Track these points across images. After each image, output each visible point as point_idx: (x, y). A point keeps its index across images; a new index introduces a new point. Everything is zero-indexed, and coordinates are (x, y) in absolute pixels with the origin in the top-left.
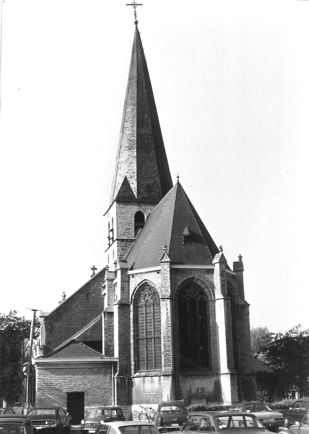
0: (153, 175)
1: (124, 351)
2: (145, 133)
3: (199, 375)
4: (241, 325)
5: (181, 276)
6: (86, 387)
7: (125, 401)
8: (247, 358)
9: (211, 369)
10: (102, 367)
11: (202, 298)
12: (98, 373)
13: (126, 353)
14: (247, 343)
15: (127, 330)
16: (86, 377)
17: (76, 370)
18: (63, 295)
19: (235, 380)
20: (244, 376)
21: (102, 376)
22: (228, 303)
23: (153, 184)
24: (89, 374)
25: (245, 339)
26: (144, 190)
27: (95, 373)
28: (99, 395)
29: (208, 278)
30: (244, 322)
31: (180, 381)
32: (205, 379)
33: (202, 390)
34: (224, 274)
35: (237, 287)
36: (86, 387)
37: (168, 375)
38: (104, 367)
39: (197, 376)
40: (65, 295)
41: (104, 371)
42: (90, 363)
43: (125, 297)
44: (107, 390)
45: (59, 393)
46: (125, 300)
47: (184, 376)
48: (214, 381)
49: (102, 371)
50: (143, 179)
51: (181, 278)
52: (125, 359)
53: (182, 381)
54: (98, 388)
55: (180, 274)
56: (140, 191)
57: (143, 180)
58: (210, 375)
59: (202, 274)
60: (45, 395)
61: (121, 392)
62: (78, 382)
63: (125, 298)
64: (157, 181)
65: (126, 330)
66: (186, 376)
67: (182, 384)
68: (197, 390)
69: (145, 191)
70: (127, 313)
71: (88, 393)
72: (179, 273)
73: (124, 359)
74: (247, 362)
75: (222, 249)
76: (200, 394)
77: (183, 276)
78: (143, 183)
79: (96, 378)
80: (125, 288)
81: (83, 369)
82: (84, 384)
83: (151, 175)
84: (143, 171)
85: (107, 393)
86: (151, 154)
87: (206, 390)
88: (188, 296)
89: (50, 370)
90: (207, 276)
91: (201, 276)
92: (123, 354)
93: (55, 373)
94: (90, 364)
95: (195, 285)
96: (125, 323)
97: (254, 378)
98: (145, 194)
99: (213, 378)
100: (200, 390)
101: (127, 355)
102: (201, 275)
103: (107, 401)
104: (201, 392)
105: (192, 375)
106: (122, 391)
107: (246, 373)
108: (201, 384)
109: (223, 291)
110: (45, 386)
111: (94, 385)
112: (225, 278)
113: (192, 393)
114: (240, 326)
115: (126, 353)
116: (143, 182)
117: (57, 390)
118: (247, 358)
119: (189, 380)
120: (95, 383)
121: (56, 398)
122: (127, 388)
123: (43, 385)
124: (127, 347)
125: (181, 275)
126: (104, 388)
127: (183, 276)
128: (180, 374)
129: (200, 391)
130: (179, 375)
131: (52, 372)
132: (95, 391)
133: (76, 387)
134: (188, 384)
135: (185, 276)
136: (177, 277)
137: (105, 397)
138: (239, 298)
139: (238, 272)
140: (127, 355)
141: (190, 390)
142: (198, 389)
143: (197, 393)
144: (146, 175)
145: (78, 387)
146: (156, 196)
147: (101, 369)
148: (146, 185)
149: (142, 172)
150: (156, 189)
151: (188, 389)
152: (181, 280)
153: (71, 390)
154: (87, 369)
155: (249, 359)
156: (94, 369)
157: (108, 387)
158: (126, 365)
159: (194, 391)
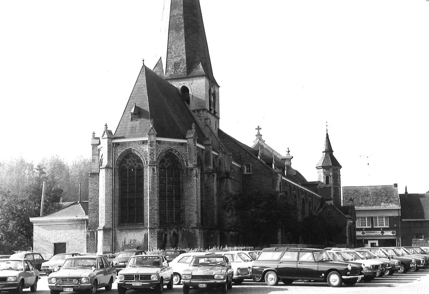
0: (181, 53)
1: (94, 210)
2: (177, 14)
3: (133, 229)
4: (190, 185)
5: (121, 149)
6: (67, 239)
7: (94, 249)
8: (193, 213)
9: (143, 225)
10: (79, 223)
11: (139, 166)
12: (76, 228)
13: (96, 212)
14: (193, 201)
15: (97, 193)
16: (67, 231)
17: (60, 226)
18: (287, 150)
19: (155, 233)
20: (190, 229)
21: (78, 231)
22: (153, 169)
23: (180, 61)
24: (70, 229)
25: (192, 197)
26: (172, 67)
27: (74, 228)
28: (77, 245)
29: (143, 149)
30: (192, 182)
31: (117, 234)
32: (137, 232)
33: (134, 241)
34: (153, 144)
35: (188, 152)
36: (67, 239)
37: (101, 230)
38: (80, 223)
39: (131, 230)
40: (289, 150)
41: (80, 226)
42: (69, 221)
43: (96, 167)
44: (82, 241)
45: (48, 244)
46: (96, 169)
47: (120, 230)
48: (144, 234)
49: (79, 227)
50: (172, 58)
51: (121, 150)
52: (94, 216)
53: (119, 234)
54: (76, 240)
55: (120, 147)
56: (169, 70)
57: (171, 59)
58: (142, 229)
59: (138, 146)
60: (39, 245)
61: (91, 242)
62: (61, 235)
63: (96, 168)
64: (184, 58)
65: (96, 194)
66: (121, 230)
67: (118, 238)
68: (130, 241)
69: (172, 68)
70: (97, 180)
71: (68, 244)
72: (119, 146)
73: (93, 217)
74: (192, 217)
75: (107, 127)
76: (132, 245)
77: (122, 148)
78: (171, 61)
79: (74, 232)
80: (95, 160)
81: (65, 225)
82: (65, 236)
83: (179, 53)
84: (173, 51)
85: (82, 243)
86: (181, 34)
87: (137, 241)
88: (128, 165)
89: (42, 226)
90: (142, 147)
91: (137, 147)
92: (93, 213)
93: (46, 229)
94: (69, 221)
95: (134, 155)
96: (95, 189)
97: (198, 231)
98: (172, 71)
99: (143, 231)
100: (132, 241)
101: (97, 213)
102: (137, 146)
103: (82, 250)
104: (133, 243)
105: (126, 229)
106: (91, 242)
107: (191, 226)
108: (133, 237)
109: (152, 158)
110: (39, 238)
111: (73, 237)
112: (154, 148)
113: (126, 244)
114: (189, 186)
115: (96, 212)
116: (172, 60)
117: (46, 241)
118: (193, 213)
119: (124, 233)
120: (73, 236)
121: (46, 247)
122: (95, 239)
123: (37, 237)
124: (97, 207)
125: (121, 148)
126: (80, 239)
127: (122, 148)
128: (117, 228)
129: (132, 243)
130: (116, 229)
131: (43, 228)
132: (74, 241)
133: (60, 239)
134: (123, 237)
135: (124, 148)
136: (117, 150)
137: (81, 247)
138: (189, 162)
139: (189, 139)
140: (97, 213)
141: (124, 242)
142: (131, 240)
143: (130, 244)
144: (175, 53)
145: (61, 239)
146: (182, 72)
147: (78, 225)
148: (173, 63)
149: (172, 51)
150: (182, 65)
151: (123, 240)
152: (120, 151)
153: (56, 241)
154: (68, 225)
155: (194, 214)
156: (73, 225)
157: (83, 239)
158: (94, 221)
159: (127, 242)
